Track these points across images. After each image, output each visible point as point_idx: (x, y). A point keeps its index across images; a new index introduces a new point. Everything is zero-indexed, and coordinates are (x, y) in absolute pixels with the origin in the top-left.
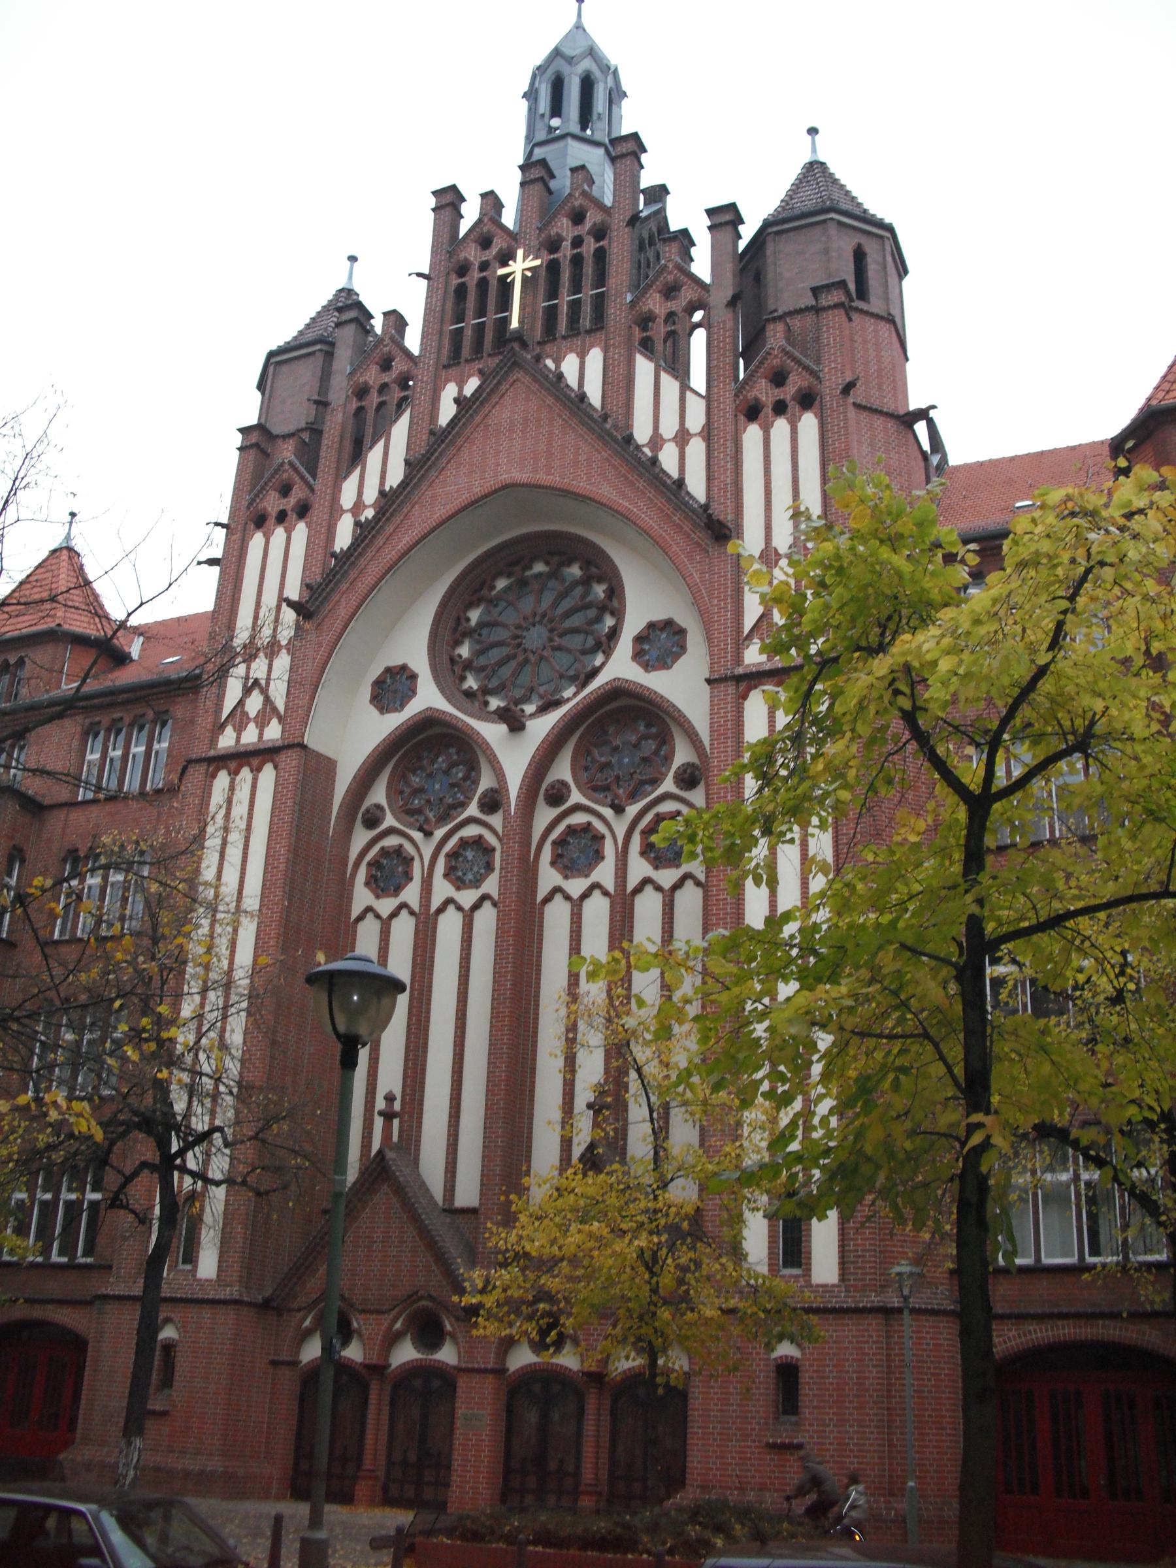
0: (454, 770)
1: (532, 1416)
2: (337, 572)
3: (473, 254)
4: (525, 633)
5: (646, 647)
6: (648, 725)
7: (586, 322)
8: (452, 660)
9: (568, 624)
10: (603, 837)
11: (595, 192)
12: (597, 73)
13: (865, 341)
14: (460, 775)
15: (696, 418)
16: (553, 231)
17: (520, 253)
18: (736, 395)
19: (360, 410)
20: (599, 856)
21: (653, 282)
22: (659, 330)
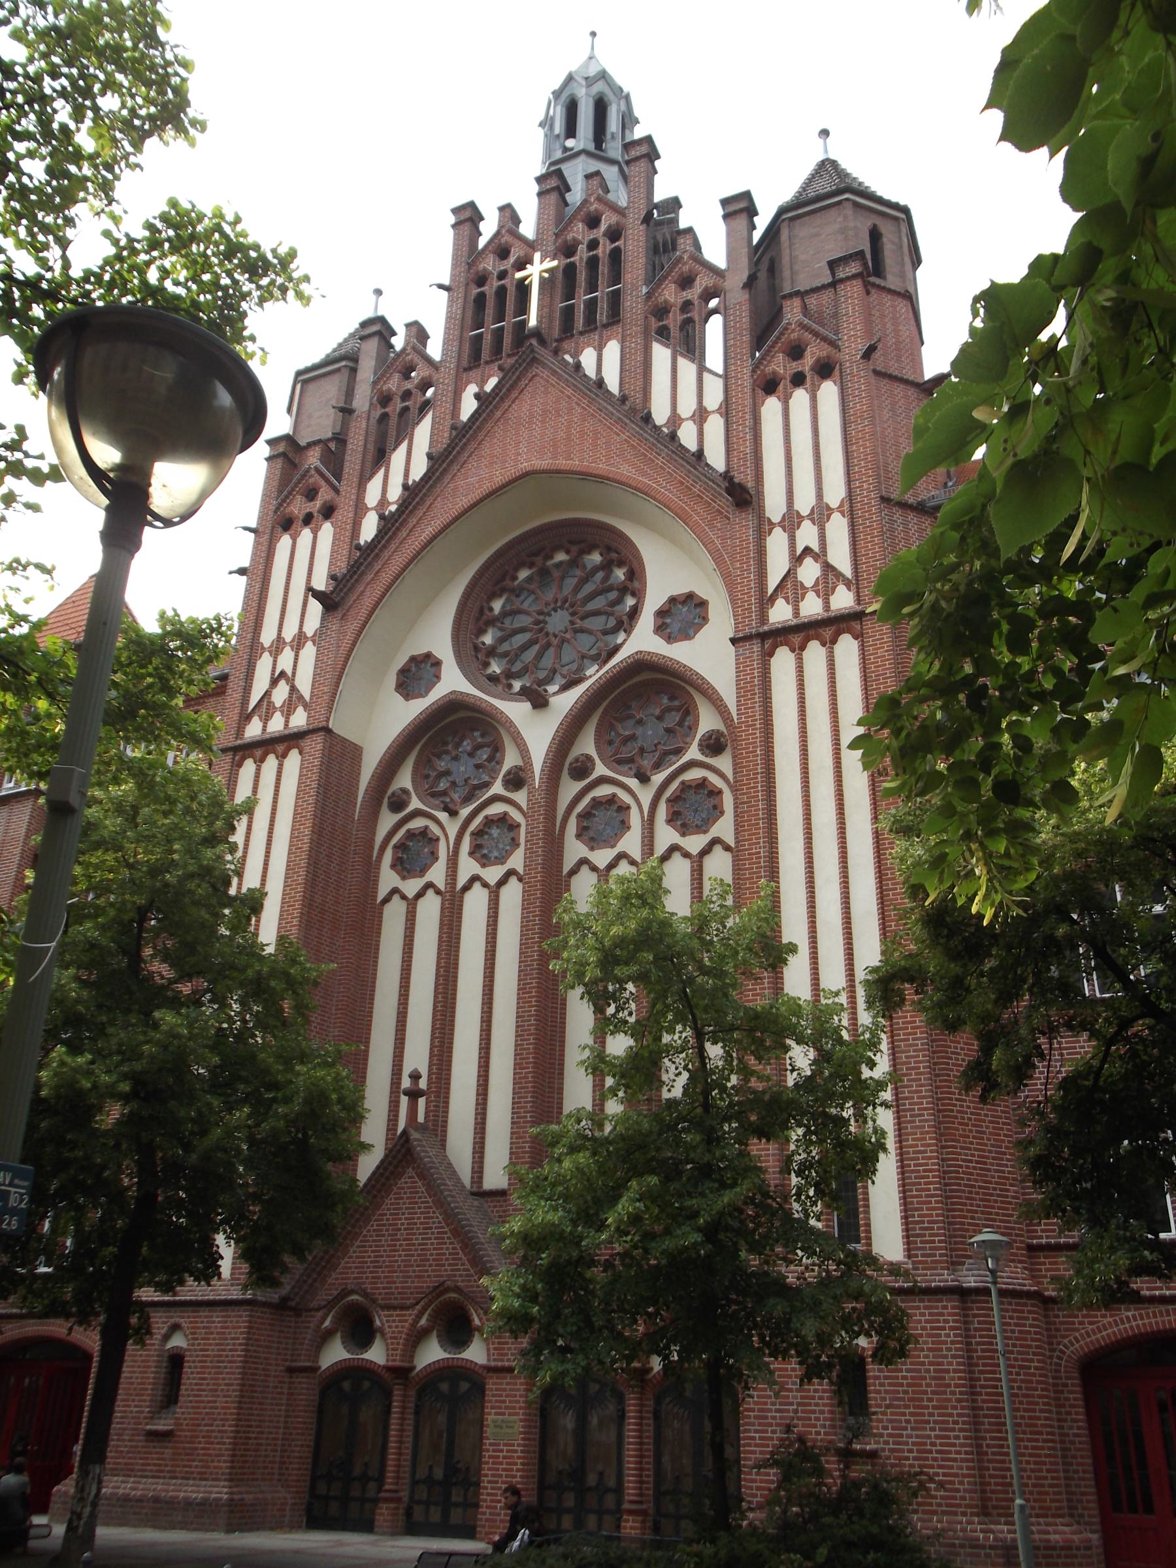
0: (479, 752)
1: (568, 1421)
2: (362, 564)
3: (490, 264)
4: (547, 618)
5: (668, 621)
6: (672, 698)
7: (602, 316)
8: (476, 648)
9: (591, 606)
10: (628, 808)
11: (611, 196)
12: (610, 96)
13: (883, 316)
14: (485, 757)
15: (714, 395)
16: (570, 237)
17: (537, 256)
18: (754, 371)
19: (384, 417)
20: (625, 826)
21: (668, 274)
22: (674, 320)
